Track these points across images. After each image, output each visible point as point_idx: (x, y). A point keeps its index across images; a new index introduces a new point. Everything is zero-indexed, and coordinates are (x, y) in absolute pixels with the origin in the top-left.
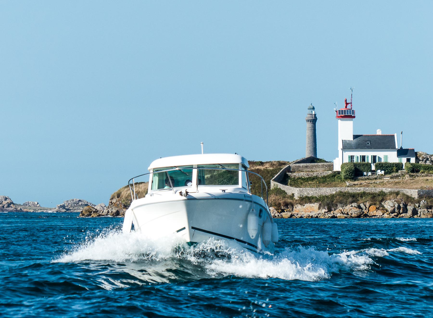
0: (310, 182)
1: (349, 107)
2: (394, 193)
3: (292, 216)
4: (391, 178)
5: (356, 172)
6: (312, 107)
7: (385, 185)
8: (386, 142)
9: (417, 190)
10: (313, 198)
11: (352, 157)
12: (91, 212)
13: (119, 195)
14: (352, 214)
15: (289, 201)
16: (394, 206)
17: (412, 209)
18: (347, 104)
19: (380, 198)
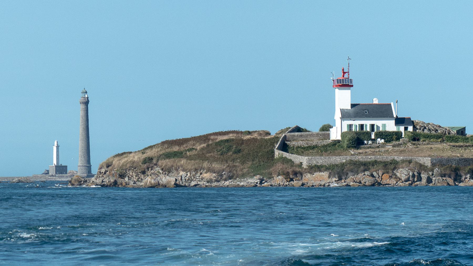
0: (311, 151)
1: (346, 76)
2: (406, 161)
3: (303, 185)
4: (394, 146)
5: (357, 140)
7: (390, 152)
8: (383, 111)
9: (430, 159)
11: (362, 126)
12: (81, 182)
13: (108, 165)
14: (365, 183)
15: (298, 169)
16: (409, 174)
17: (426, 177)
18: (344, 73)
19: (392, 167)
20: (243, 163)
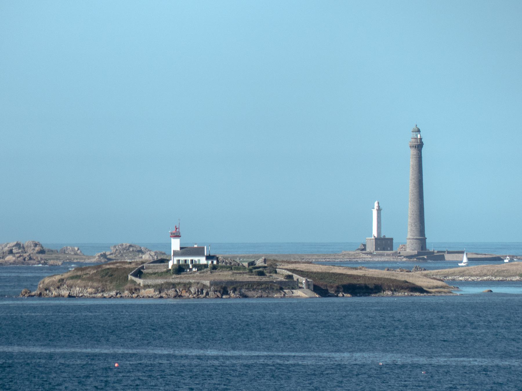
1: (177, 230)
4: (200, 273)
5: (180, 269)
6: (417, 130)
8: (199, 252)
10: (151, 285)
15: (137, 287)
18: (176, 229)
19: (188, 286)
20: (111, 282)
